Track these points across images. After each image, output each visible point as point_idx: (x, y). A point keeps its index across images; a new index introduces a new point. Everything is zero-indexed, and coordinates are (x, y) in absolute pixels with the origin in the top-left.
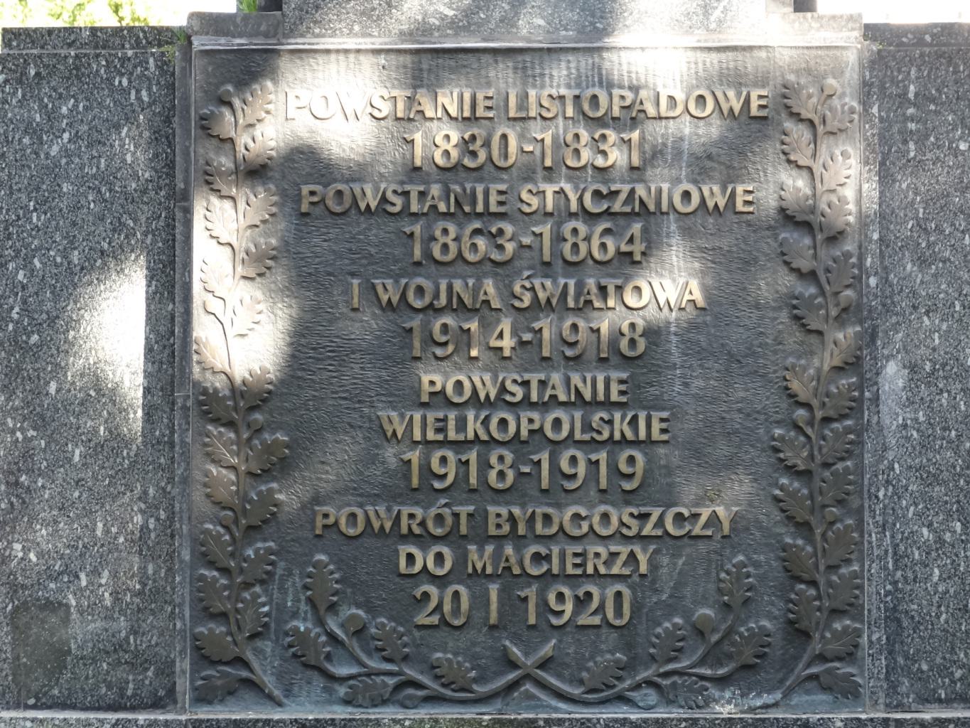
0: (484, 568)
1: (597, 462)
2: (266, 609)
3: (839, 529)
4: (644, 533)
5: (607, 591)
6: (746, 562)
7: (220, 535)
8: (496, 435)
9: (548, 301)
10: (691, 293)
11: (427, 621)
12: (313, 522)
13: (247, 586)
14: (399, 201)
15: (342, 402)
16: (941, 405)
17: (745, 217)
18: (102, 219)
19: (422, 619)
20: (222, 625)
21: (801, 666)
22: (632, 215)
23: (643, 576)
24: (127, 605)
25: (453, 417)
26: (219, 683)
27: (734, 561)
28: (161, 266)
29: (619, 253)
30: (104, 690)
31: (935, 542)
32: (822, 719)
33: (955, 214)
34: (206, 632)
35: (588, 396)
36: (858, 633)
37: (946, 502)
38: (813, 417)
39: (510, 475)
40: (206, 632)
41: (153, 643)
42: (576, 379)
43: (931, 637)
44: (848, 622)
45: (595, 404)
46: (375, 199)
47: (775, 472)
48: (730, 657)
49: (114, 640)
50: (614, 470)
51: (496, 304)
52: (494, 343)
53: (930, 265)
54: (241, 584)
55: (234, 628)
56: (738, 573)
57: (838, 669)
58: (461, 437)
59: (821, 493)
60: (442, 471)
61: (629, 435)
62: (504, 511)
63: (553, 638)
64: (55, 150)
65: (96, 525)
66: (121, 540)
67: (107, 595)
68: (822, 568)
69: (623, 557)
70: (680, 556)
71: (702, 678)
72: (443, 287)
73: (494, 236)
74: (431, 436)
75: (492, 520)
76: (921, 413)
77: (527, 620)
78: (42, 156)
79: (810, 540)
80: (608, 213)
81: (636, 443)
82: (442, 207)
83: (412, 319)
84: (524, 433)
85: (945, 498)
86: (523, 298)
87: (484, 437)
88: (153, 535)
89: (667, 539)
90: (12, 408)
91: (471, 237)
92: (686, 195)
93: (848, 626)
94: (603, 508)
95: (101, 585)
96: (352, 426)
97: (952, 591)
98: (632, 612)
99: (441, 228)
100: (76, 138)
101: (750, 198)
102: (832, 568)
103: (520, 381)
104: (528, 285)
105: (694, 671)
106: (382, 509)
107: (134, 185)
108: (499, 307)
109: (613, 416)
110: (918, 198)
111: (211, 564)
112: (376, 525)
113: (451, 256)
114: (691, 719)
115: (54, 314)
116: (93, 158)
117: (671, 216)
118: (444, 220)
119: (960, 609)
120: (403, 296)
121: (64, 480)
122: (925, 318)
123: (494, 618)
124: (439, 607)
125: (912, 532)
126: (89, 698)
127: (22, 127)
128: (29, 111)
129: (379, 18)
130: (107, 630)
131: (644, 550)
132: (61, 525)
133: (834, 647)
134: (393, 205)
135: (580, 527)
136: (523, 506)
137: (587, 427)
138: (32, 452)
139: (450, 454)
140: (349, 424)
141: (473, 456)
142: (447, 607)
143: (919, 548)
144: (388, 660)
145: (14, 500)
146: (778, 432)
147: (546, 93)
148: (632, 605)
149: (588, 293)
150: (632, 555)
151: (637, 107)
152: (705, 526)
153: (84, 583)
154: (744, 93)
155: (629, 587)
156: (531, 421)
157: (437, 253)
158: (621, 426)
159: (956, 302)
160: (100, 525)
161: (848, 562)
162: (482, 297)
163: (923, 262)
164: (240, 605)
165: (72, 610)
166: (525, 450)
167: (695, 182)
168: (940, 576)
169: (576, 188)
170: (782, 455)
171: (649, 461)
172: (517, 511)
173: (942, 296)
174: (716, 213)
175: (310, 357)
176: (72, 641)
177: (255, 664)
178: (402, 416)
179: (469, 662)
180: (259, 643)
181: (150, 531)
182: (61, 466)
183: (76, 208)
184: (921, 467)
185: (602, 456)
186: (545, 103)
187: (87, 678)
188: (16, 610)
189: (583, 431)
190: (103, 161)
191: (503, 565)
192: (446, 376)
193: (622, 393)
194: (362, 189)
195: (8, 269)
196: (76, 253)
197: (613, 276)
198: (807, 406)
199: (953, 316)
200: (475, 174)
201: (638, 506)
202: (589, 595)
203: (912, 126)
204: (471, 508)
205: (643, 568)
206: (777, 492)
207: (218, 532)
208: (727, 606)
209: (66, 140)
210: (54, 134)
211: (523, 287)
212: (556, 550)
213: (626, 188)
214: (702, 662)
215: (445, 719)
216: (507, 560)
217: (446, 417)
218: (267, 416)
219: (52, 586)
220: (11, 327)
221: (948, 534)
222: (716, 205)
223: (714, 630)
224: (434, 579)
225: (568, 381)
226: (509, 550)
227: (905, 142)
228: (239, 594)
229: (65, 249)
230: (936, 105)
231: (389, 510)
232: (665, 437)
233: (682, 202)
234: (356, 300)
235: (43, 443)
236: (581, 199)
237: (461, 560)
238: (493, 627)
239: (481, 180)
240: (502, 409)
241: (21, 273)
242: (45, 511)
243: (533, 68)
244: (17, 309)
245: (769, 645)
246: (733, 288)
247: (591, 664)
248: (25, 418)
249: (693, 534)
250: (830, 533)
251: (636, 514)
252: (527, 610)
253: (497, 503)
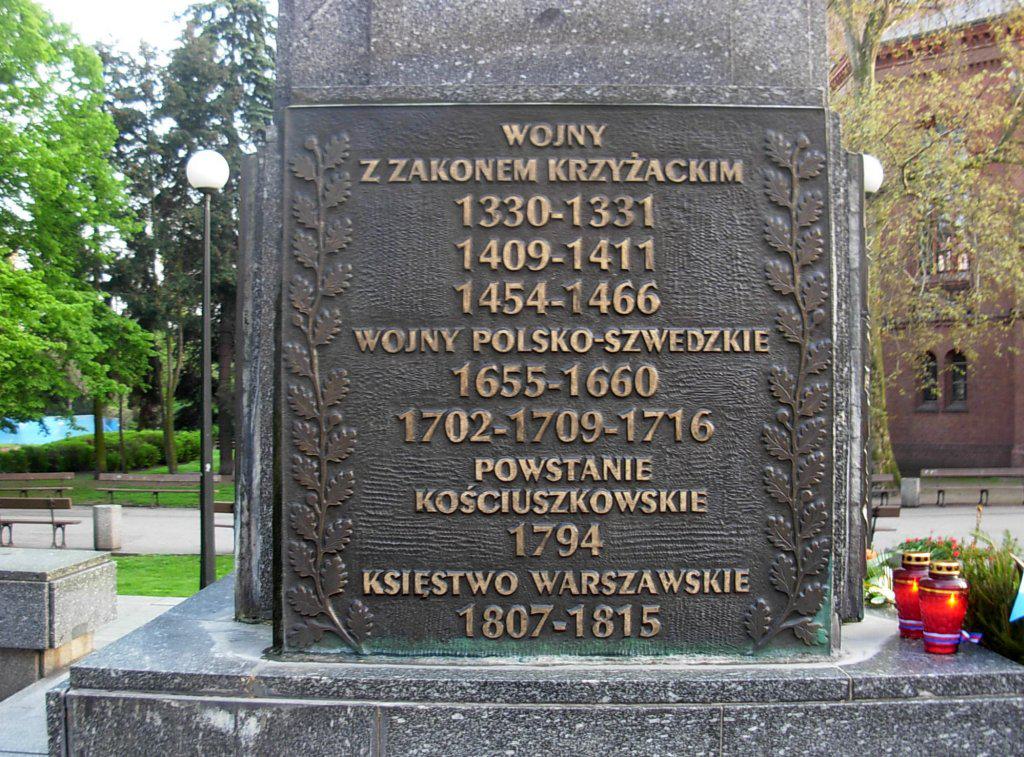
29: (525, 307)
61: (673, 508)
106: (628, 494)
154: (666, 332)
198: (788, 406)
202: (479, 417)
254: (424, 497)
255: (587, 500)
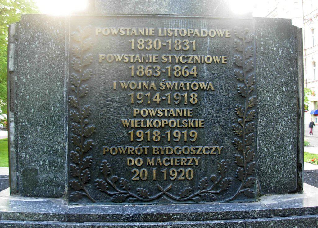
0: (152, 164)
1: (184, 134)
2: (89, 175)
3: (250, 152)
4: (197, 153)
5: (187, 170)
6: (225, 161)
7: (76, 154)
8: (155, 126)
9: (170, 88)
10: (210, 86)
11: (136, 179)
12: (102, 151)
13: (84, 169)
14: (127, 59)
15: (111, 116)
16: (270, 116)
17: (224, 65)
18: (46, 65)
19: (133, 178)
20: (77, 180)
21: (239, 189)
22: (193, 64)
23: (196, 166)
24: (53, 170)
25: (143, 121)
26: (77, 196)
27: (222, 161)
28: (62, 77)
29: (190, 74)
30: (47, 192)
31: (268, 152)
32: (253, 211)
33: (273, 66)
34: (73, 182)
35: (181, 115)
36: (254, 180)
37: (271, 141)
38: (243, 121)
39: (159, 137)
40: (73, 182)
41: (60, 180)
42: (178, 110)
43: (266, 176)
44: (252, 177)
45: (183, 117)
46: (120, 58)
47: (233, 136)
48: (220, 187)
49: (50, 179)
50: (188, 135)
51: (155, 88)
52: (154, 99)
53: (267, 79)
54: (83, 168)
55: (80, 181)
56: (223, 164)
57: (249, 190)
58: (145, 127)
59: (245, 142)
60: (140, 136)
61: (193, 126)
62: (157, 148)
63: (171, 183)
64: (33, 46)
65: (44, 148)
66: (51, 152)
67: (48, 167)
68: (245, 163)
69: (191, 161)
70: (207, 160)
71: (212, 193)
72: (140, 83)
73: (154, 69)
74: (136, 126)
75: (154, 150)
76: (265, 118)
77: (164, 178)
78: (30, 48)
79: (242, 155)
80: (186, 63)
81: (195, 128)
82: (140, 61)
83: (131, 92)
84: (163, 125)
85: (271, 140)
86: (163, 87)
87: (152, 127)
88: (60, 151)
89: (203, 155)
90: (22, 116)
91: (148, 69)
92: (209, 58)
93: (252, 178)
94: (185, 147)
95: (46, 164)
96: (114, 123)
97: (272, 164)
98: (194, 176)
99: (139, 66)
100: (39, 43)
101: (226, 60)
102: (248, 163)
103: (162, 110)
104: (164, 83)
105: (210, 191)
106: (122, 147)
107: (55, 56)
108: (156, 89)
109: (188, 120)
110: (264, 62)
111: (74, 163)
112: (121, 152)
113: (142, 75)
114: (215, 212)
115: (33, 90)
116: (44, 48)
117: (204, 64)
118: (140, 64)
119: (273, 169)
120: (128, 86)
121: (36, 136)
122: (266, 93)
123: (154, 178)
124: (139, 175)
125: (262, 149)
126: (44, 194)
127: (25, 40)
128: (27, 36)
129: (122, 8)
130: (48, 176)
131: (197, 158)
132: (35, 148)
133: (248, 184)
134: (126, 60)
135: (179, 152)
136: (163, 146)
137: (181, 124)
138: (27, 128)
139: (142, 132)
140: (113, 123)
141: (148, 132)
142: (141, 175)
143: (264, 154)
144: (124, 190)
145: (22, 141)
146: (234, 125)
147: (169, 29)
148: (193, 174)
149: (181, 86)
150: (194, 159)
151: (195, 34)
152: (214, 152)
153: (41, 164)
155: (193, 169)
156: (165, 122)
157: (138, 73)
158: (190, 123)
159: (273, 89)
160: (45, 148)
161: (252, 161)
162: (151, 86)
163: (265, 79)
164: (82, 174)
165: (39, 171)
166: (163, 130)
167: (211, 55)
168: (269, 161)
169: (177, 56)
170: (235, 131)
171: (198, 134)
172: (161, 148)
173: (270, 88)
174: (217, 64)
175: (102, 103)
176: (39, 179)
177: (87, 191)
178: (128, 120)
179: (147, 190)
180: (88, 185)
181: (59, 150)
182: (35, 132)
183: (39, 62)
184: (265, 132)
185: (185, 132)
186: (169, 32)
187: (43, 189)
188: (23, 170)
189: (180, 125)
190: (46, 49)
191: (157, 163)
192: (141, 109)
193: (191, 114)
194: (117, 55)
195: (21, 78)
196: (39, 74)
197: (188, 81)
198: (242, 118)
199: (272, 93)
200: (149, 51)
201: (195, 146)
203: (262, 43)
204: (148, 147)
205: (197, 164)
206: (233, 142)
207: (75, 153)
208: (219, 173)
209: (37, 44)
210: (34, 42)
211: (163, 84)
212: (172, 159)
213: (192, 56)
214: (212, 189)
215: (142, 214)
216: (158, 162)
217: (141, 121)
218: (90, 120)
219: (33, 164)
220: (21, 94)
221: (271, 150)
222: (217, 61)
223: (216, 180)
224: (137, 167)
225: (175, 111)
226: (159, 159)
227: (260, 47)
228: (82, 171)
229: (36, 73)
230: (268, 38)
231: (124, 147)
232: (203, 127)
233: (207, 60)
234: (115, 87)
235: (30, 126)
236: (179, 59)
237: (145, 161)
238: (154, 180)
239: (151, 53)
240: (157, 118)
241: (24, 79)
242: (31, 144)
243: (166, 22)
244: (23, 89)
245: (231, 184)
246: (222, 85)
247: (182, 190)
248: (25, 119)
249: (211, 154)
250: (247, 153)
251: (195, 148)
252: (164, 175)
253: (155, 145)
254: (191, 122)
255: (152, 122)
